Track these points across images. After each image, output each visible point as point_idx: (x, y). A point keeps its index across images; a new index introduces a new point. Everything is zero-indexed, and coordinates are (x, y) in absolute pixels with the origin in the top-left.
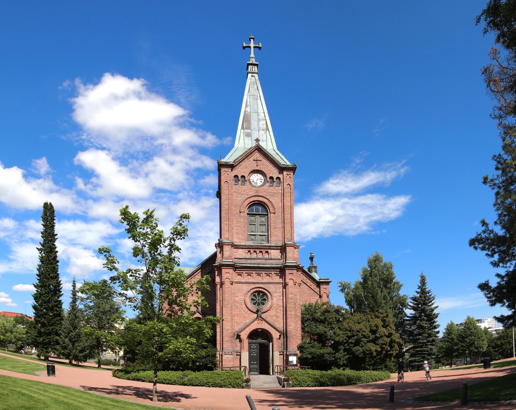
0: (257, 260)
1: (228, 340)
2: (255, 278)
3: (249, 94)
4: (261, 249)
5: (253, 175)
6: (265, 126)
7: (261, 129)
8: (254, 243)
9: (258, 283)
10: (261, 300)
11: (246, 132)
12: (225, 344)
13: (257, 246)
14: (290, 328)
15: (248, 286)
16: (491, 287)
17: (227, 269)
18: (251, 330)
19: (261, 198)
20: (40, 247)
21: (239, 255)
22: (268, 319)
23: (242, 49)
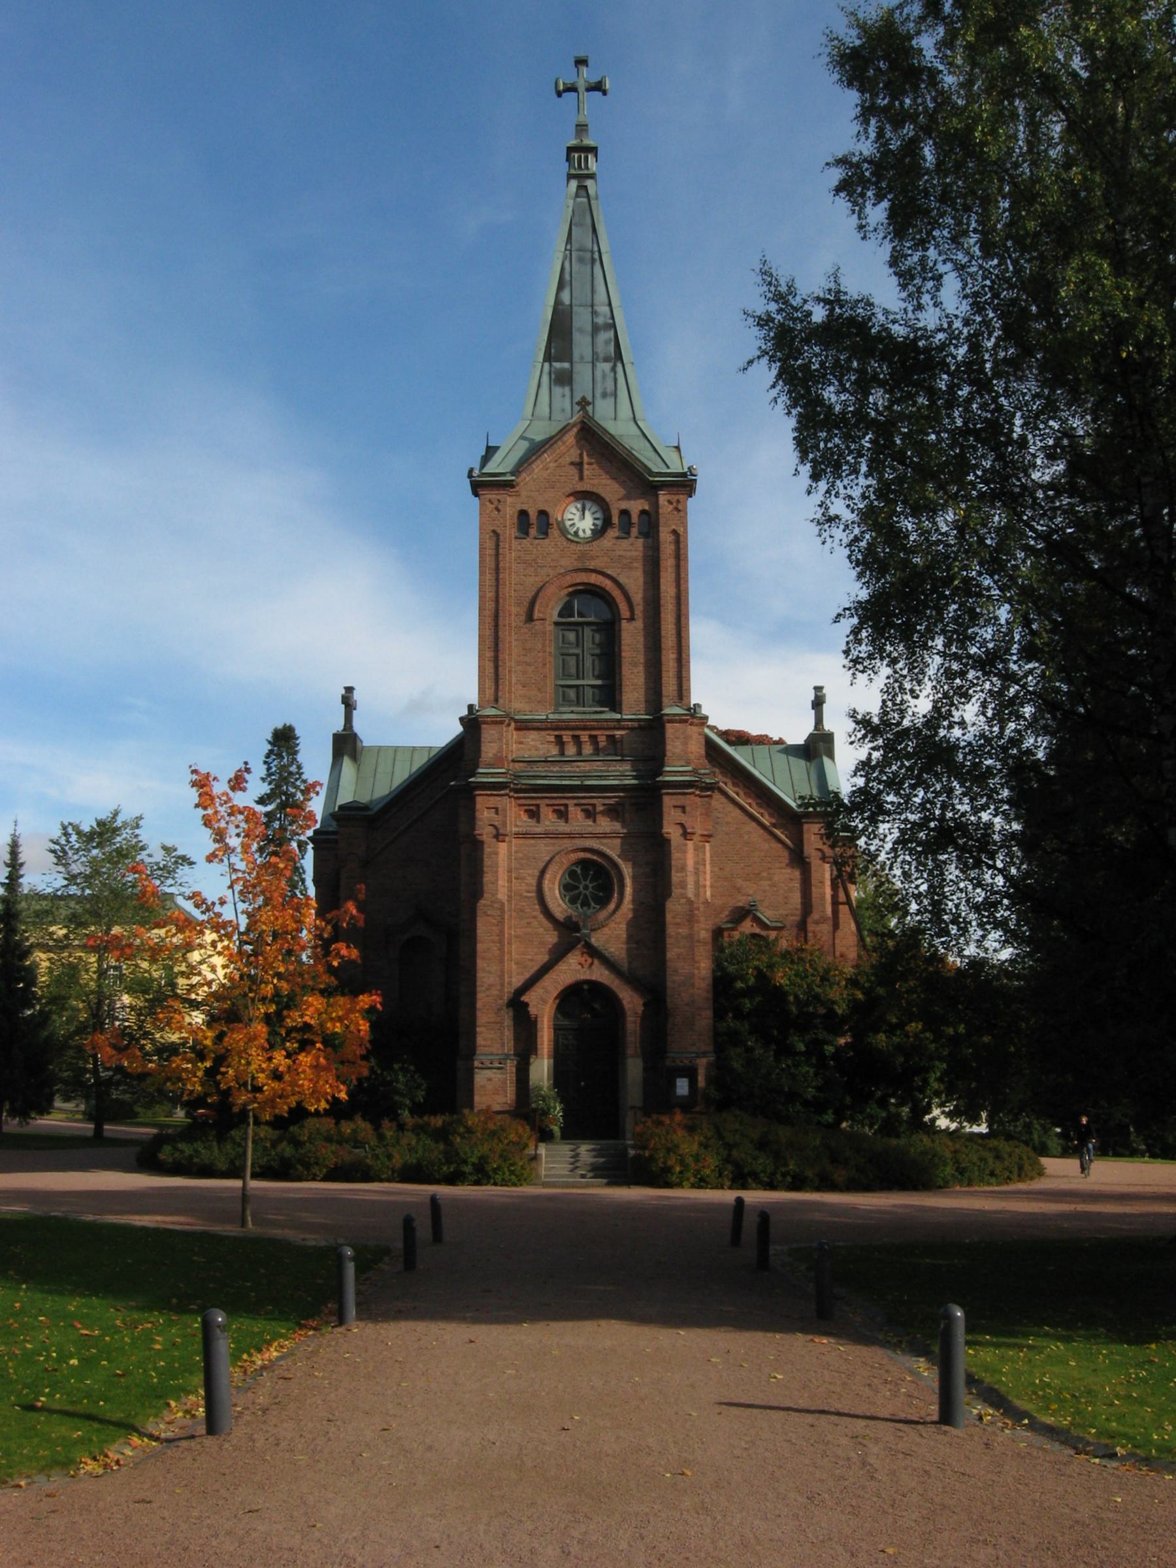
0: (579, 764)
1: (492, 1020)
2: (538, 830)
3: (569, 247)
5: (572, 505)
7: (601, 356)
8: (572, 712)
9: (581, 836)
10: (585, 895)
12: (482, 1033)
13: (582, 720)
14: (674, 982)
15: (553, 844)
17: (492, 798)
18: (560, 988)
19: (594, 575)
21: (530, 750)
22: (612, 950)
23: (556, 96)
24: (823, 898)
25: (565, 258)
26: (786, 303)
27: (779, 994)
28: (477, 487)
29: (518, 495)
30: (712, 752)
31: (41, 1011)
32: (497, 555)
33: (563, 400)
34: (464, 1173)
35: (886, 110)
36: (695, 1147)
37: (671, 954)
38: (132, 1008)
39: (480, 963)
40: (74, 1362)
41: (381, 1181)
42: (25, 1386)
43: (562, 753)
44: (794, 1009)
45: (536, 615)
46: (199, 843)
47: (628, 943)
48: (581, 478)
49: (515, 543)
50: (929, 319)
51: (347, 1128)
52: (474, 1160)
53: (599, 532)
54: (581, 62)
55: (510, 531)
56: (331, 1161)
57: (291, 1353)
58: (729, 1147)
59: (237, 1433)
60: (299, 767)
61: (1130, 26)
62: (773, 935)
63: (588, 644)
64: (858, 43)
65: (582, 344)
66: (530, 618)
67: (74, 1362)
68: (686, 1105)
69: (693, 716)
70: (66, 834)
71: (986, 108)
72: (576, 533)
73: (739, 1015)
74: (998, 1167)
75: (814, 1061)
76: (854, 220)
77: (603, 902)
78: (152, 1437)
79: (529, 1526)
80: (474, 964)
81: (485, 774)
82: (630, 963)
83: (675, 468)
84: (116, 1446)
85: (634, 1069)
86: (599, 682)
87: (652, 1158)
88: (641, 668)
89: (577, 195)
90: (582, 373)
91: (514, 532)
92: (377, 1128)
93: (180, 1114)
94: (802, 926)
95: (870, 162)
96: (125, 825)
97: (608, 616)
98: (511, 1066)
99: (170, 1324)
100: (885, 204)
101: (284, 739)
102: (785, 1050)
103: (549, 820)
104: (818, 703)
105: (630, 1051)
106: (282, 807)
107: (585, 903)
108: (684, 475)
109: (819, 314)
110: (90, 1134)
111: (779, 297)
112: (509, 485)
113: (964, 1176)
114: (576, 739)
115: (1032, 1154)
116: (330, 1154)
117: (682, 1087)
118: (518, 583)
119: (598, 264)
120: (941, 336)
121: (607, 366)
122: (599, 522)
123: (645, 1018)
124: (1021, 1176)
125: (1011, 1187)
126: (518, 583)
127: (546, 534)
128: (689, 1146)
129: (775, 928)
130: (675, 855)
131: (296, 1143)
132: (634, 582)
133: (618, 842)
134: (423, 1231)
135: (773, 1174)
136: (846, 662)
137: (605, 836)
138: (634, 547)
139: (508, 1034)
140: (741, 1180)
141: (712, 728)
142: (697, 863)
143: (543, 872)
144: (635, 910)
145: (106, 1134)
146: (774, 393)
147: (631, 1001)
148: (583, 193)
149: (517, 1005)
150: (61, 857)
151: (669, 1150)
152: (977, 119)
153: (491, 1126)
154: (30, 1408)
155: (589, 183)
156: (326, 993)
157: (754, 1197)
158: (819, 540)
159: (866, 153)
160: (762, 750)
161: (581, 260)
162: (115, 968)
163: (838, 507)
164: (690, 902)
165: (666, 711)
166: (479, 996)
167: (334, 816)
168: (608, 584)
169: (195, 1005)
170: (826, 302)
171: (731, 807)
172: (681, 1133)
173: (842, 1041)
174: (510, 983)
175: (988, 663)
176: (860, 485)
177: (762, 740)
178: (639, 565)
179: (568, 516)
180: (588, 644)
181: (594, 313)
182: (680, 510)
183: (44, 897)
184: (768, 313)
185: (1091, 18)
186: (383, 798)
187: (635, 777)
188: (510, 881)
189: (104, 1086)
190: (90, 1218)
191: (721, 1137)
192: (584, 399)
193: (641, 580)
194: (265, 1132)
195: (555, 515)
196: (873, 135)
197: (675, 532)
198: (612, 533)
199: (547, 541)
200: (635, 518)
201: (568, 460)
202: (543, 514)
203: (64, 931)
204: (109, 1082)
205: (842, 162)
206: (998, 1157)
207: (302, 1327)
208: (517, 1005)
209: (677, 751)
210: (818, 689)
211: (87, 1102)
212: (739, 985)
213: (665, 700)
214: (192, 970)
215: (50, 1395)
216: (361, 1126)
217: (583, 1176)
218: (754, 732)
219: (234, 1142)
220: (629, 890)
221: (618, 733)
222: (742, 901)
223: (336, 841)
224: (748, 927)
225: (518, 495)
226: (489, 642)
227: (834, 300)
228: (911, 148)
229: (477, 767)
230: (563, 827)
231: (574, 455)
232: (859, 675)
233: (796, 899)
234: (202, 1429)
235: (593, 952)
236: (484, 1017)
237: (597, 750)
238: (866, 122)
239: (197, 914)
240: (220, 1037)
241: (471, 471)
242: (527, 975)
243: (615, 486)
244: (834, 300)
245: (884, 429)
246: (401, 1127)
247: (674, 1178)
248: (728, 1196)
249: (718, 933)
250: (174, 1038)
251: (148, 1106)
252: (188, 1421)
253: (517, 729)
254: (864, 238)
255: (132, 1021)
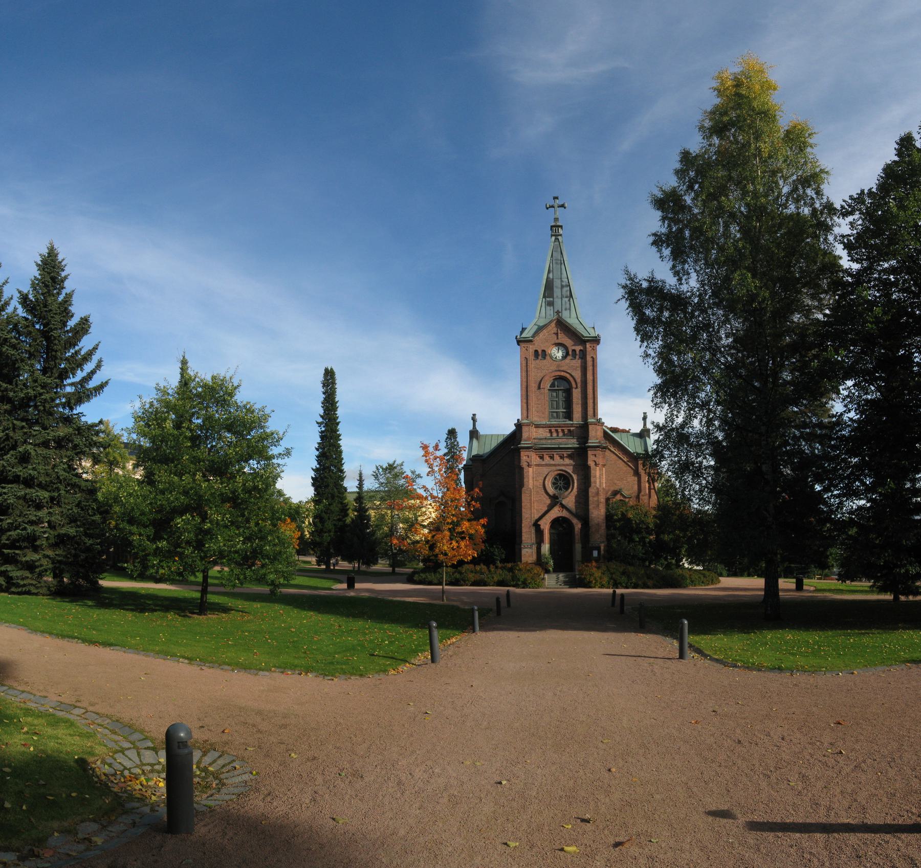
2: (543, 463)
4: (563, 427)
6: (568, 293)
7: (565, 296)
11: (548, 301)
16: (299, 506)
20: (320, 420)
24: (645, 487)
25: (550, 262)
26: (633, 281)
27: (629, 520)
28: (519, 342)
29: (534, 344)
30: (606, 435)
31: (372, 530)
32: (527, 366)
33: (550, 311)
34: (519, 585)
35: (671, 218)
36: (600, 574)
37: (591, 507)
38: (403, 528)
39: (523, 510)
40: (387, 642)
41: (490, 586)
42: (371, 649)
43: (551, 436)
44: (634, 525)
45: (541, 387)
46: (424, 469)
47: (575, 503)
48: (558, 338)
49: (533, 362)
50: (684, 288)
51: (478, 568)
52: (522, 580)
53: (564, 357)
54: (555, 198)
55: (531, 357)
56: (473, 580)
57: (460, 640)
58: (612, 574)
59: (442, 662)
60: (458, 443)
61: (763, 200)
62: (627, 500)
63: (561, 397)
64: (662, 196)
65: (557, 292)
66: (539, 388)
67: (387, 642)
68: (597, 560)
69: (599, 422)
70: (378, 469)
71: (708, 220)
72: (556, 358)
73: (615, 529)
74: (705, 580)
75: (641, 544)
76: (659, 255)
77: (567, 489)
78: (413, 664)
79: (543, 687)
80: (521, 510)
81: (523, 444)
82: (576, 510)
83: (593, 334)
84: (401, 666)
85: (578, 547)
86: (565, 410)
87: (585, 578)
88: (580, 406)
89: (555, 241)
90: (558, 302)
91: (533, 358)
92: (488, 568)
93: (421, 564)
94: (638, 497)
95: (665, 235)
96: (398, 465)
97: (568, 387)
98: (534, 547)
99: (419, 632)
100: (670, 249)
101: (452, 433)
102: (631, 540)
103: (547, 459)
104: (645, 418)
105: (577, 541)
106: (452, 457)
107: (560, 489)
108: (596, 337)
109: (645, 285)
110: (391, 571)
111: (631, 279)
112: (531, 341)
113: (693, 583)
114: (557, 431)
115: (716, 575)
116: (472, 577)
117: (595, 553)
118: (535, 376)
119: (563, 266)
120: (689, 294)
121: (567, 299)
122: (564, 354)
123: (581, 529)
124: (712, 583)
125: (709, 587)
126: (535, 376)
127: (545, 358)
128: (598, 574)
129: (628, 498)
130: (592, 472)
131: (461, 573)
132: (577, 375)
133: (572, 467)
134: (503, 602)
135: (627, 583)
136: (652, 404)
137: (567, 465)
138: (577, 363)
139: (533, 536)
140: (616, 585)
141: (606, 427)
142: (600, 475)
143: (545, 479)
144: (578, 491)
145: (396, 571)
146: (628, 311)
147: (578, 525)
148: (557, 240)
149: (536, 525)
150: (376, 477)
151: (591, 575)
152: (705, 223)
153: (528, 568)
154: (373, 655)
155: (559, 238)
156: (469, 520)
157: (619, 591)
158: (643, 363)
159: (663, 232)
160: (624, 435)
161: (557, 263)
162: (397, 515)
163: (650, 352)
164: (598, 489)
165: (589, 420)
166: (523, 521)
167: (470, 459)
168: (568, 376)
169: (424, 527)
170: (648, 281)
171: (612, 455)
172: (595, 569)
173: (652, 537)
174: (534, 517)
175: (704, 405)
176: (658, 344)
177: (624, 431)
178: (579, 369)
179: (553, 352)
180: (561, 397)
181: (562, 281)
182: (594, 349)
183: (372, 491)
184: (626, 284)
185: (749, 196)
186: (487, 453)
187: (578, 444)
188: (533, 481)
189: (394, 555)
190: (391, 598)
191: (609, 570)
192: (558, 311)
193: (580, 374)
194: (450, 569)
195: (548, 351)
196: (666, 225)
197: (592, 357)
198: (569, 358)
199: (545, 361)
200: (578, 353)
201: (553, 332)
202: (544, 351)
203: (379, 503)
204: (396, 554)
205: (655, 235)
206: (705, 577)
207: (463, 632)
208: (536, 525)
209: (593, 435)
210: (645, 413)
211: (390, 561)
212: (615, 517)
213: (589, 417)
214: (424, 513)
215: (379, 651)
216: (483, 567)
217: (560, 585)
218: (621, 428)
219: (439, 573)
220: (576, 484)
221: (572, 428)
222: (617, 488)
223: (471, 468)
224: (618, 497)
225: (534, 344)
226: (524, 397)
227: (651, 280)
228: (680, 231)
229: (521, 441)
230: (552, 462)
231: (555, 330)
232: (657, 409)
233: (636, 487)
234: (430, 662)
235: (563, 506)
236: (524, 530)
237: (564, 435)
238: (664, 222)
239: (424, 494)
240: (433, 537)
241: (516, 337)
242: (540, 515)
243: (570, 341)
244: (651, 280)
245: (668, 324)
246: (497, 567)
247: (593, 585)
248: (611, 591)
249: (607, 500)
250: (418, 538)
251: (410, 562)
252: (425, 660)
253: (535, 427)
254: (662, 261)
255: (403, 533)
